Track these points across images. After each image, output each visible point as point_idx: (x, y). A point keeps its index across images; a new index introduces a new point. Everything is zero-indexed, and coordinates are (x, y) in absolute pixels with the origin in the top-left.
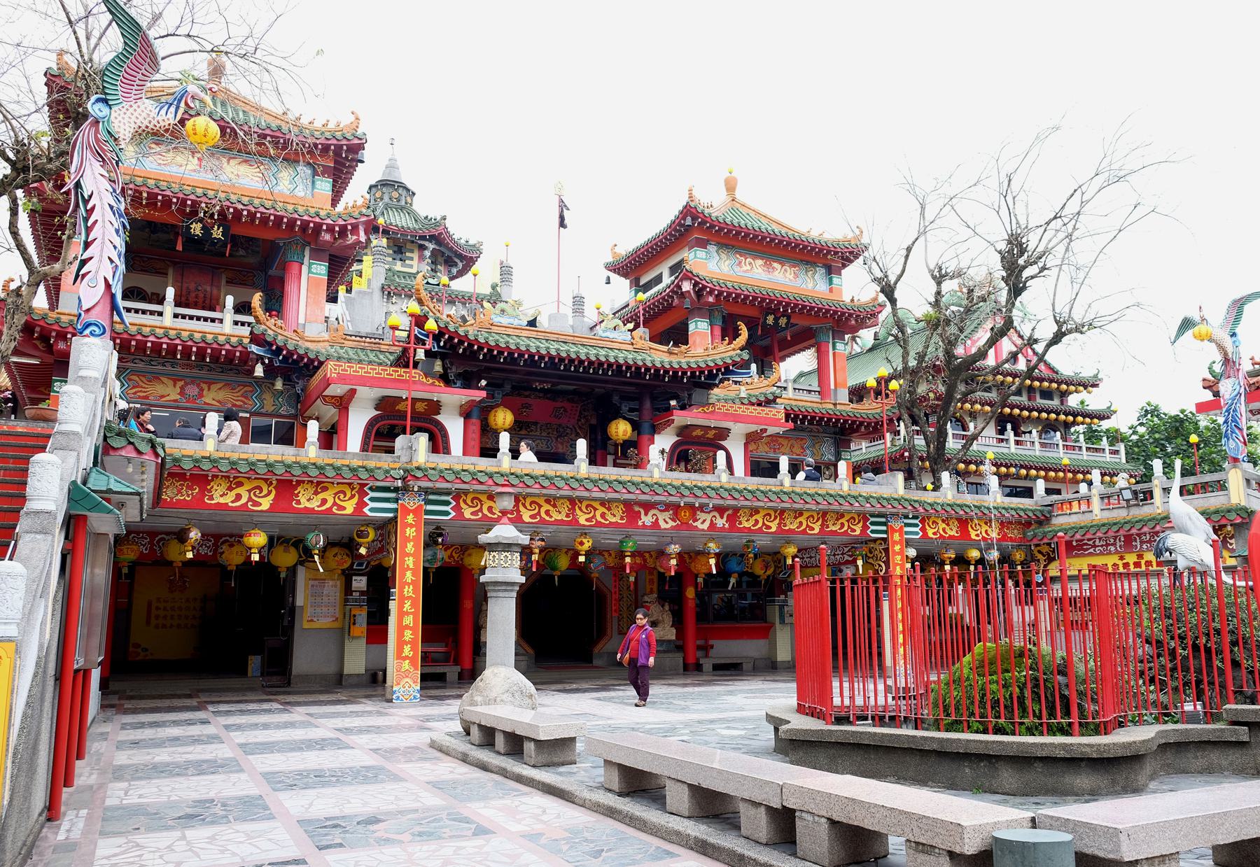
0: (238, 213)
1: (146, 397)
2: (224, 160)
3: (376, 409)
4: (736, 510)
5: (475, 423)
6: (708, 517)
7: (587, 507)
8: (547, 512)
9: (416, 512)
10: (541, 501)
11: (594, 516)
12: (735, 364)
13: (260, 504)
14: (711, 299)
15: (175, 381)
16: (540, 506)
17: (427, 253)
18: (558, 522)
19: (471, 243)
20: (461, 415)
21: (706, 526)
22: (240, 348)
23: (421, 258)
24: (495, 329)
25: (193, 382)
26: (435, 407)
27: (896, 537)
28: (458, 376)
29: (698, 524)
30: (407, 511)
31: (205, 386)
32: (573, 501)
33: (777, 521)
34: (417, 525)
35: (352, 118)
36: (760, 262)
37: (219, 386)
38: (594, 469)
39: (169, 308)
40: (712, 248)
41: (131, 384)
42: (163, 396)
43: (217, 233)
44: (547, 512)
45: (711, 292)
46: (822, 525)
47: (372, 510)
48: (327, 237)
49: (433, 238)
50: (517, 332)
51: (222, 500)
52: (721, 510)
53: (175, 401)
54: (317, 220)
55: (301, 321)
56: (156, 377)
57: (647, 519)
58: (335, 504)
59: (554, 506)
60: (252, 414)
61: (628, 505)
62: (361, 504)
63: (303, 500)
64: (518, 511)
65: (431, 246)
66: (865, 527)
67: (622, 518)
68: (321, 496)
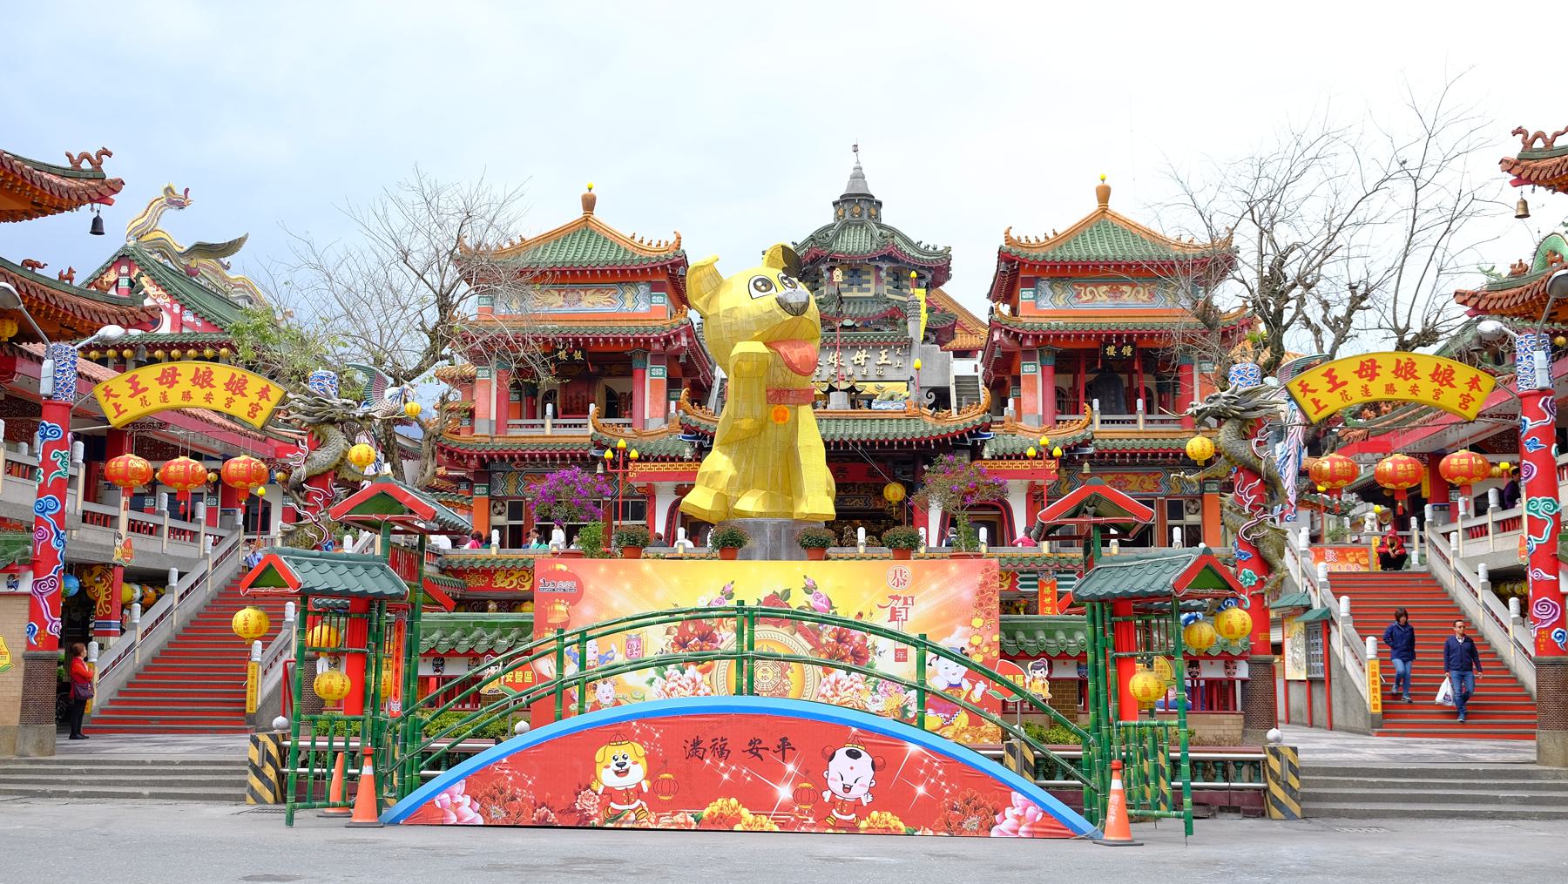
0: (586, 340)
14: (1029, 343)
17: (883, 274)
19: (940, 249)
23: (879, 280)
27: (1047, 590)
30: (1043, 585)
36: (1105, 288)
39: (548, 422)
43: (578, 355)
48: (657, 347)
49: (883, 258)
65: (885, 266)
66: (1014, 583)
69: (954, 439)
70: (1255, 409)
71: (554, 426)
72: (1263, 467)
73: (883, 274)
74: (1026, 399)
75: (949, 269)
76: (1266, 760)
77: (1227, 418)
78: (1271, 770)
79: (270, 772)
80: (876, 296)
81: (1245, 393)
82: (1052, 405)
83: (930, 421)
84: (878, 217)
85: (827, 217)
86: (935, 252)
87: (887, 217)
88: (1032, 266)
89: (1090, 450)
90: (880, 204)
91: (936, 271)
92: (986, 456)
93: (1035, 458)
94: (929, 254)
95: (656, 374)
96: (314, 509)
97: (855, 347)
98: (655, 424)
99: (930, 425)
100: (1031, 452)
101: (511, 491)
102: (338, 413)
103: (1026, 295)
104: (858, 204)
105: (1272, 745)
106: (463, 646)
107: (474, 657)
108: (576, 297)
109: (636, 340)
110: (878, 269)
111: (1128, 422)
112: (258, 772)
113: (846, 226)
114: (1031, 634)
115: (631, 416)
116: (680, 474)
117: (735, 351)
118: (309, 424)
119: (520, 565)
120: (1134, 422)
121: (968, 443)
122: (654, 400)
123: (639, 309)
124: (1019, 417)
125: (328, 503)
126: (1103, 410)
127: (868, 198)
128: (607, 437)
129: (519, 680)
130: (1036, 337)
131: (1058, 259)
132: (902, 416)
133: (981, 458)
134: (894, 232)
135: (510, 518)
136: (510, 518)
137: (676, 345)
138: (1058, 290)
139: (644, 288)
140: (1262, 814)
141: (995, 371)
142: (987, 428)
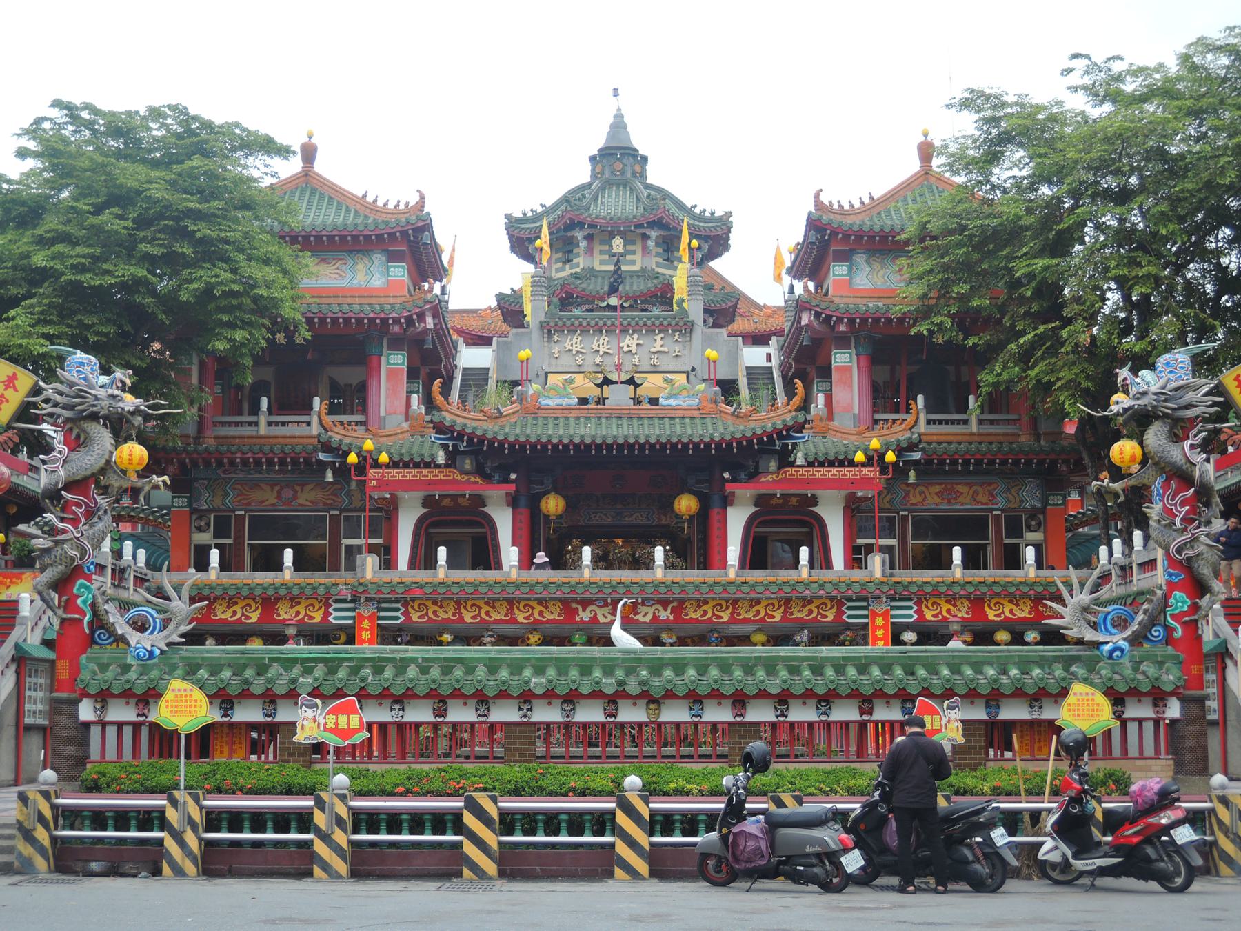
1: (249, 504)
3: (756, 505)
4: (682, 602)
5: (524, 512)
6: (651, 611)
7: (525, 606)
8: (487, 613)
9: (371, 618)
10: (481, 603)
11: (532, 615)
12: (788, 429)
13: (249, 618)
14: (843, 328)
15: (272, 486)
16: (480, 608)
17: (651, 244)
18: (549, 621)
21: (648, 619)
23: (645, 249)
25: (287, 486)
26: (479, 501)
27: (879, 621)
28: (495, 469)
29: (640, 617)
31: (298, 488)
32: (511, 602)
33: (730, 610)
34: (371, 629)
35: (417, 199)
37: (311, 486)
40: (860, 259)
44: (487, 613)
45: (840, 320)
46: (785, 612)
47: (335, 618)
48: (396, 329)
50: (566, 413)
51: (223, 616)
52: (664, 603)
54: (383, 315)
55: (382, 413)
56: (256, 485)
57: (585, 615)
58: (306, 615)
59: (493, 607)
60: (342, 511)
61: (565, 604)
62: (327, 614)
63: (282, 613)
64: (460, 613)
65: (654, 234)
67: (560, 615)
68: (295, 609)
69: (760, 440)
70: (1189, 406)
71: (270, 424)
72: (1197, 474)
73: (651, 244)
74: (839, 394)
75: (728, 238)
76: (1213, 810)
77: (1157, 417)
78: (1220, 823)
79: (42, 835)
80: (643, 270)
81: (1177, 389)
82: (867, 404)
83: (730, 421)
84: (643, 175)
85: (582, 174)
86: (713, 218)
87: (655, 176)
88: (847, 236)
89: (917, 456)
90: (645, 159)
91: (715, 237)
92: (800, 461)
93: (387, 466)
94: (706, 220)
95: (395, 361)
96: (75, 522)
97: (624, 331)
98: (396, 422)
99: (724, 426)
100: (860, 457)
101: (218, 503)
102: (104, 407)
103: (838, 270)
104: (618, 160)
105: (1220, 793)
106: (258, 686)
107: (270, 699)
110: (645, 237)
111: (959, 422)
112: (28, 836)
113: (607, 185)
114: (933, 669)
115: (364, 411)
116: (430, 483)
118: (67, 420)
119: (245, 592)
120: (966, 422)
121: (774, 447)
122: (393, 392)
123: (374, 281)
124: (830, 416)
125: (90, 514)
126: (929, 408)
127: (631, 153)
128: (337, 438)
129: (343, 725)
130: (852, 321)
131: (877, 228)
132: (696, 414)
133: (792, 464)
134: (666, 195)
135: (215, 537)
136: (215, 537)
137: (419, 327)
138: (877, 265)
139: (379, 258)
140: (156, 872)
141: (796, 359)
142: (800, 428)
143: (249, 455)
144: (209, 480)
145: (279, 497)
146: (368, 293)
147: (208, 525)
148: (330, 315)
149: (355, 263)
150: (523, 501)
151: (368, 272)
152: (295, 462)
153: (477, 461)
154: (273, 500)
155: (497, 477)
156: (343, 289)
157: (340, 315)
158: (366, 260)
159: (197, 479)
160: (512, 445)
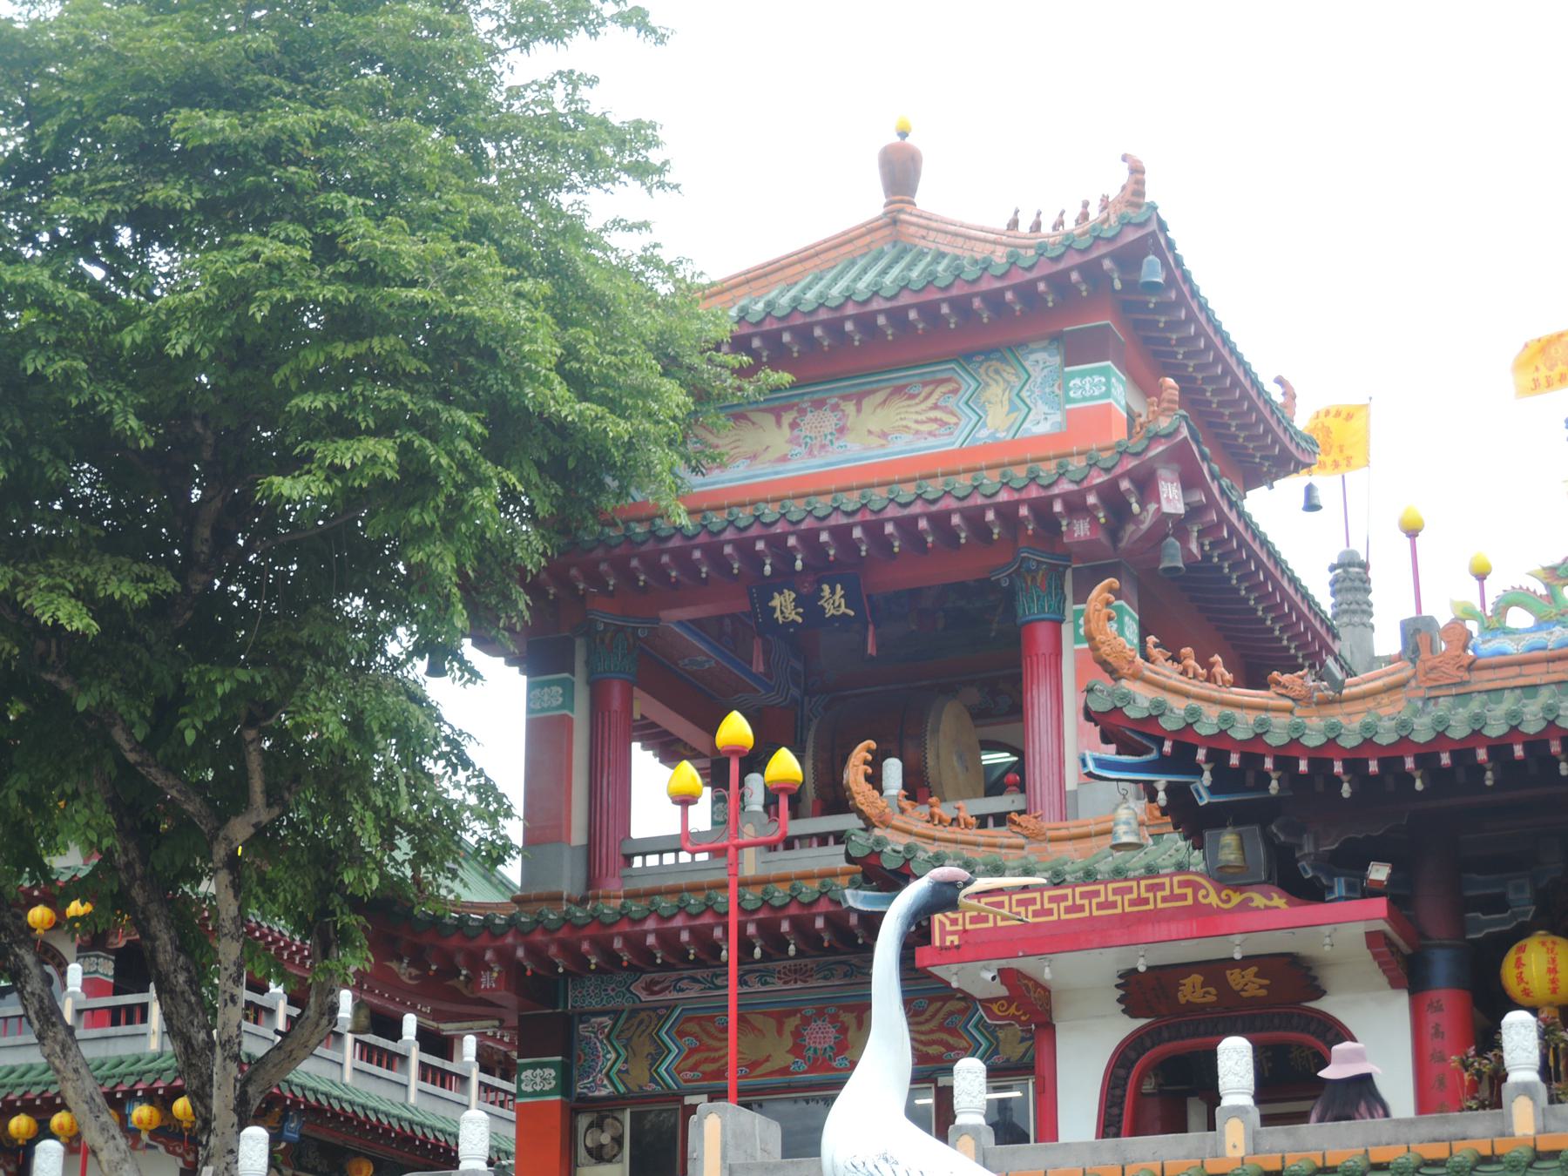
2: (850, 407)
3: (1131, 1011)
15: (780, 1018)
20: (1395, 984)
22: (824, 906)
24: (1482, 680)
25: (820, 1013)
35: (1122, 175)
38: (1279, 1137)
41: (688, 1041)
42: (753, 1065)
43: (834, 602)
48: (1081, 530)
53: (785, 1071)
54: (1034, 493)
55: (1071, 784)
101: (640, 1077)
108: (829, 421)
109: (1007, 513)
117: (22, 952)
123: (1042, 416)
139: (1042, 361)
143: (678, 922)
144: (616, 1014)
145: (797, 1050)
146: (1002, 457)
147: (618, 1141)
148: (892, 511)
149: (982, 386)
150: (1441, 964)
151: (1019, 404)
152: (802, 926)
153: (1269, 840)
154: (782, 1058)
155: (1340, 887)
156: (962, 453)
157: (917, 508)
158: (1009, 373)
159: (585, 1016)
160: (1355, 763)
